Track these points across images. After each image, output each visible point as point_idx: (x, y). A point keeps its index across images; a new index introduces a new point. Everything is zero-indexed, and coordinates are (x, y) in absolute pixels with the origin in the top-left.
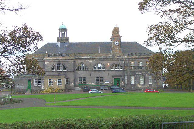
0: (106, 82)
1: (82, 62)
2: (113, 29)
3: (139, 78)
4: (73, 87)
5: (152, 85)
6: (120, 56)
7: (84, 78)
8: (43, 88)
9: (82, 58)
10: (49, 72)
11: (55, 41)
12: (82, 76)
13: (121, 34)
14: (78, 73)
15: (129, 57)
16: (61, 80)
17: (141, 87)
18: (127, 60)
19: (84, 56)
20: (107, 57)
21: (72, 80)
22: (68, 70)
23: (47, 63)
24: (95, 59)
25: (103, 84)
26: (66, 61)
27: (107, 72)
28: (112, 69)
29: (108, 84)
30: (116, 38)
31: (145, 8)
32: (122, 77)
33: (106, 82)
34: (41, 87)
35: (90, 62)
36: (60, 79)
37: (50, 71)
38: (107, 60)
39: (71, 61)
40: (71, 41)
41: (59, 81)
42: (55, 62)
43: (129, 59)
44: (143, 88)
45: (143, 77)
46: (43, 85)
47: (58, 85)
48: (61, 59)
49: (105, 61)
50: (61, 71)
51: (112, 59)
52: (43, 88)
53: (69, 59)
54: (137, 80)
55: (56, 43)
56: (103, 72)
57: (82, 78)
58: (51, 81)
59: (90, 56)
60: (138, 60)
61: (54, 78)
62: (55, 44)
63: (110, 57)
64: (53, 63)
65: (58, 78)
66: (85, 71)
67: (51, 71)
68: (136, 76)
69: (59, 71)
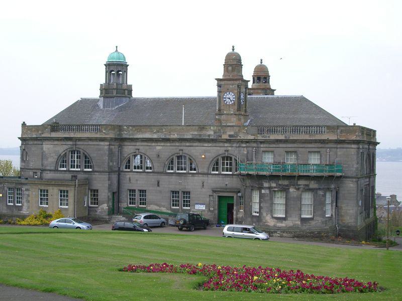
0: (198, 207)
1: (137, 147)
2: (223, 62)
3: (271, 199)
5: (313, 223)
6: (237, 134)
7: (143, 192)
8: (25, 211)
9: (137, 139)
10: (50, 170)
11: (94, 93)
12: (137, 187)
14: (128, 176)
16: (67, 191)
17: (274, 226)
18: (255, 145)
19: (143, 132)
20: (200, 135)
21: (104, 194)
22: (96, 169)
26: (90, 143)
27: (198, 179)
29: (203, 211)
30: (228, 84)
32: (239, 194)
33: (198, 207)
34: (20, 208)
37: (53, 168)
38: (202, 144)
39: (102, 143)
41: (64, 194)
42: (66, 147)
43: (261, 143)
44: (279, 229)
45: (284, 195)
46: (25, 204)
47: (61, 205)
48: (80, 139)
49: (197, 148)
50: (79, 169)
51: (213, 141)
52: (25, 211)
53: (96, 139)
54: (267, 202)
56: (190, 178)
57: (137, 193)
58: (64, 196)
59: (158, 132)
60: (284, 145)
61: (51, 188)
63: (209, 136)
64: (62, 148)
65: (62, 188)
66: (144, 172)
67: (56, 170)
68: (263, 191)
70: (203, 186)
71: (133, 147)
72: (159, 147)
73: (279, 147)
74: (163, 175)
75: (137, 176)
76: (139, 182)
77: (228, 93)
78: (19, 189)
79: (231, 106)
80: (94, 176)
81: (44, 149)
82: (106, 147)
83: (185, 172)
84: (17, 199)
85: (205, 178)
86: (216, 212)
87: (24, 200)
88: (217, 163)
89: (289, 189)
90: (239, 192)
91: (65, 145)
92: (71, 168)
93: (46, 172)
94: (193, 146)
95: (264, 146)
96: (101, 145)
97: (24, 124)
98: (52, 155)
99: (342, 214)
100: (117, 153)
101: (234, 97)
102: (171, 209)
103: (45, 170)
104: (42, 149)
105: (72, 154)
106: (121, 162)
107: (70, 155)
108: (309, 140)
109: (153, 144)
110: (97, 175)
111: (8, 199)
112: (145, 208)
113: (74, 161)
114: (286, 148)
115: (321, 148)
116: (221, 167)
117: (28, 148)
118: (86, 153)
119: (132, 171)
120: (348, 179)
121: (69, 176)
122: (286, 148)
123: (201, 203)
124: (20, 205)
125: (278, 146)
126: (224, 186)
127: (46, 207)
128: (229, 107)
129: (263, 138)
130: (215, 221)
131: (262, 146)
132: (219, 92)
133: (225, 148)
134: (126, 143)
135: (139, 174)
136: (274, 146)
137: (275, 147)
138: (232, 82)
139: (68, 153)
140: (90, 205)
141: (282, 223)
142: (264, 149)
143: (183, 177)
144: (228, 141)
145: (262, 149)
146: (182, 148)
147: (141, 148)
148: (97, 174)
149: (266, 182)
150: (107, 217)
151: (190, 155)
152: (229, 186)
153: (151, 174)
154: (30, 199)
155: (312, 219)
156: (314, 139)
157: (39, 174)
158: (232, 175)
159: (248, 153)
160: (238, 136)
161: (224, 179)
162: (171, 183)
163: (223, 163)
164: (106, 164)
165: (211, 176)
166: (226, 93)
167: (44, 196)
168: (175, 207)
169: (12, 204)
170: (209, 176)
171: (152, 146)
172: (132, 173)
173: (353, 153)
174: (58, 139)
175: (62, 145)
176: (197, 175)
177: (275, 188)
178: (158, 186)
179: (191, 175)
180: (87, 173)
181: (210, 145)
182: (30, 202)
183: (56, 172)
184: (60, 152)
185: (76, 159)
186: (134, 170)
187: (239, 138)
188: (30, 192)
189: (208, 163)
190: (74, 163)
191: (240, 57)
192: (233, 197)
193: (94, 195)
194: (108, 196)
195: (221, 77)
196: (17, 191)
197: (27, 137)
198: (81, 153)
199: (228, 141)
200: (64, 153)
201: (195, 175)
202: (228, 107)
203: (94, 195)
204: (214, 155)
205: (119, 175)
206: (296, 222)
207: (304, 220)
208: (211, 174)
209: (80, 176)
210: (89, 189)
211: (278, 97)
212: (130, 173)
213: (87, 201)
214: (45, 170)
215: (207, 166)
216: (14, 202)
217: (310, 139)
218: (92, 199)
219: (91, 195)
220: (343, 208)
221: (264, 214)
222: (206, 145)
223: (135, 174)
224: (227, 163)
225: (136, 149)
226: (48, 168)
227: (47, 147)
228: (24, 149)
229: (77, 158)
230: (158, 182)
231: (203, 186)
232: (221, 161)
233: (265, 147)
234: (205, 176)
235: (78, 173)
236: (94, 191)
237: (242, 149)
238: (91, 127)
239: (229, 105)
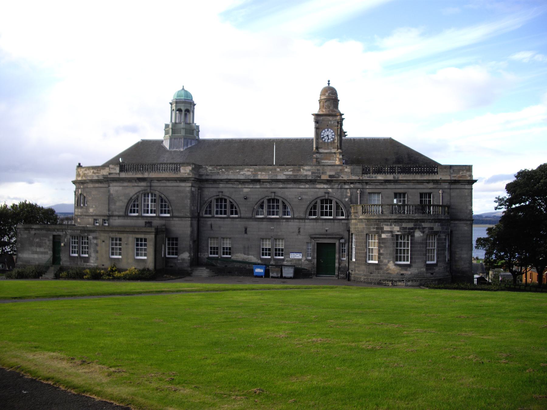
1: (219, 190)
4: (186, 265)
5: (437, 269)
6: (338, 174)
10: (119, 216)
13: (342, 108)
14: (209, 223)
15: (366, 177)
22: (176, 214)
23: (117, 191)
24: (258, 181)
25: (283, 260)
27: (294, 224)
28: (310, 214)
31: (524, 372)
32: (342, 241)
33: (293, 256)
34: (86, 260)
35: (246, 190)
36: (142, 236)
37: (122, 213)
38: (297, 186)
39: (183, 184)
40: (204, 135)
41: (140, 243)
42: (137, 189)
43: (367, 183)
46: (93, 255)
48: (159, 180)
49: (291, 190)
50: (154, 215)
55: (162, 141)
56: (284, 223)
61: (125, 235)
62: (158, 144)
64: (132, 190)
65: (139, 236)
67: (126, 216)
68: (384, 236)
69: (150, 215)
70: (299, 232)
71: (215, 190)
73: (387, 189)
74: (251, 220)
75: (220, 222)
76: (222, 229)
77: (326, 130)
78: (85, 237)
79: (329, 144)
80: (173, 222)
81: (112, 192)
82: (188, 189)
83: (278, 217)
84: (82, 248)
85: (302, 224)
86: (315, 261)
87: (92, 250)
88: (315, 207)
89: (414, 232)
90: (342, 238)
91: (138, 186)
92: (144, 213)
93: (114, 218)
94: (287, 188)
95: (370, 187)
96: (182, 186)
98: (120, 198)
99: (456, 259)
100: (197, 196)
101: (333, 134)
102: (262, 259)
103: (113, 216)
104: (109, 191)
105: (145, 196)
106: (201, 207)
107: (143, 198)
108: (420, 180)
109: (240, 186)
110: (176, 221)
111: (71, 249)
112: (230, 258)
113: (148, 205)
114: (395, 189)
115: (434, 188)
116: (318, 210)
117: (86, 192)
118: (163, 196)
119: (213, 217)
120: (463, 222)
121: (141, 222)
122: (395, 189)
123: (297, 252)
124: (87, 255)
125: (385, 187)
126: (323, 231)
127: (118, 259)
128: (328, 145)
129: (369, 179)
131: (368, 187)
132: (317, 128)
133: (325, 190)
134: (207, 185)
135: (222, 220)
136: (382, 187)
137: (384, 189)
139: (140, 196)
140: (167, 256)
141: (406, 270)
142: (370, 191)
143: (275, 223)
144: (328, 182)
145: (368, 191)
146: (274, 190)
147: (225, 190)
148: (177, 219)
149: (387, 225)
150: (189, 269)
151: (283, 198)
152: (329, 232)
153: (237, 220)
154: (98, 248)
156: (423, 179)
158: (333, 219)
159: (351, 195)
160: (339, 176)
161: (324, 224)
164: (188, 208)
165: (308, 221)
166: (324, 129)
167: (116, 244)
168: (225, 256)
169: (76, 255)
170: (306, 221)
171: (239, 188)
172: (214, 219)
173: (467, 194)
174: (130, 180)
175: (133, 186)
176: (292, 221)
177: (10, 251)
178: (246, 232)
179: (284, 220)
180: (164, 219)
181: (307, 186)
182: (99, 252)
183: (126, 218)
184: (131, 195)
185: (150, 203)
186: (216, 216)
187: (340, 178)
188: (99, 241)
189: (306, 206)
190: (148, 207)
191: (336, 91)
192: (335, 244)
193: (173, 244)
194: (190, 245)
195: (316, 112)
196: (82, 239)
197: (86, 179)
198: (157, 196)
199: (328, 182)
200: (136, 196)
201: (289, 220)
202: (326, 145)
203: (173, 244)
204: (312, 198)
205: (198, 221)
206: (422, 269)
207: (429, 267)
208: (308, 219)
209: (156, 223)
210: (166, 237)
211: (348, 139)
212: (212, 219)
213: (165, 252)
214: (113, 216)
215: (305, 209)
216: (78, 252)
217: (421, 179)
218: (169, 249)
219: (169, 244)
220: (457, 253)
222: (302, 187)
223: (218, 219)
224: (326, 208)
225: (219, 192)
226: (116, 213)
227: (115, 188)
228: (81, 194)
229: (152, 202)
231: (299, 232)
232: (319, 205)
233: (371, 188)
234: (301, 221)
235: (152, 219)
236: (173, 239)
237: (345, 190)
238: (159, 166)
239: (328, 143)
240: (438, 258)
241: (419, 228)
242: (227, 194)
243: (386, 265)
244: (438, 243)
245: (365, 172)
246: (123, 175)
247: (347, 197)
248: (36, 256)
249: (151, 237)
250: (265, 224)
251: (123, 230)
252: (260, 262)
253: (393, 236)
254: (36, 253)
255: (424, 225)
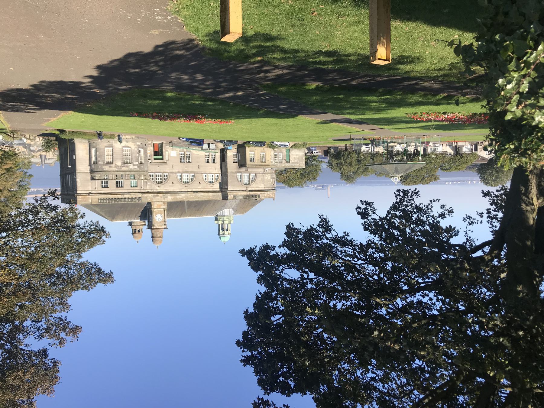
5: (106, 144)
14: (216, 171)
27: (175, 170)
35: (200, 187)
37: (258, 174)
41: (252, 160)
42: (251, 187)
56: (181, 171)
57: (211, 161)
72: (199, 188)
87: (273, 156)
97: (238, 343)
130: (164, 145)
138: (158, 227)
146: (186, 188)
152: (157, 166)
155: (106, 147)
157: (265, 171)
159: (146, 186)
162: (191, 167)
163: (161, 179)
178: (199, 166)
186: (161, 174)
188: (270, 161)
189: (170, 180)
221: (136, 149)
224: (159, 179)
230: (199, 167)
240: (104, 151)
241: (118, 167)
242: (208, 185)
243: (135, 147)
244: (105, 159)
245: (140, 198)
246: (258, 193)
247: (149, 185)
248: (297, 153)
249: (248, 162)
250: (190, 170)
251: (259, 166)
252: (191, 150)
253: (133, 163)
254: (297, 155)
255: (115, 169)
